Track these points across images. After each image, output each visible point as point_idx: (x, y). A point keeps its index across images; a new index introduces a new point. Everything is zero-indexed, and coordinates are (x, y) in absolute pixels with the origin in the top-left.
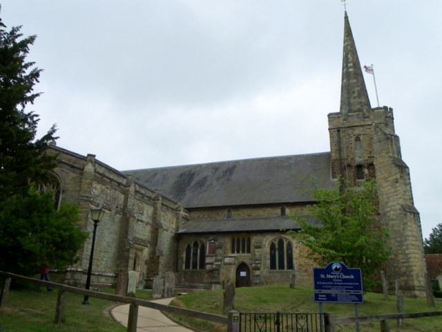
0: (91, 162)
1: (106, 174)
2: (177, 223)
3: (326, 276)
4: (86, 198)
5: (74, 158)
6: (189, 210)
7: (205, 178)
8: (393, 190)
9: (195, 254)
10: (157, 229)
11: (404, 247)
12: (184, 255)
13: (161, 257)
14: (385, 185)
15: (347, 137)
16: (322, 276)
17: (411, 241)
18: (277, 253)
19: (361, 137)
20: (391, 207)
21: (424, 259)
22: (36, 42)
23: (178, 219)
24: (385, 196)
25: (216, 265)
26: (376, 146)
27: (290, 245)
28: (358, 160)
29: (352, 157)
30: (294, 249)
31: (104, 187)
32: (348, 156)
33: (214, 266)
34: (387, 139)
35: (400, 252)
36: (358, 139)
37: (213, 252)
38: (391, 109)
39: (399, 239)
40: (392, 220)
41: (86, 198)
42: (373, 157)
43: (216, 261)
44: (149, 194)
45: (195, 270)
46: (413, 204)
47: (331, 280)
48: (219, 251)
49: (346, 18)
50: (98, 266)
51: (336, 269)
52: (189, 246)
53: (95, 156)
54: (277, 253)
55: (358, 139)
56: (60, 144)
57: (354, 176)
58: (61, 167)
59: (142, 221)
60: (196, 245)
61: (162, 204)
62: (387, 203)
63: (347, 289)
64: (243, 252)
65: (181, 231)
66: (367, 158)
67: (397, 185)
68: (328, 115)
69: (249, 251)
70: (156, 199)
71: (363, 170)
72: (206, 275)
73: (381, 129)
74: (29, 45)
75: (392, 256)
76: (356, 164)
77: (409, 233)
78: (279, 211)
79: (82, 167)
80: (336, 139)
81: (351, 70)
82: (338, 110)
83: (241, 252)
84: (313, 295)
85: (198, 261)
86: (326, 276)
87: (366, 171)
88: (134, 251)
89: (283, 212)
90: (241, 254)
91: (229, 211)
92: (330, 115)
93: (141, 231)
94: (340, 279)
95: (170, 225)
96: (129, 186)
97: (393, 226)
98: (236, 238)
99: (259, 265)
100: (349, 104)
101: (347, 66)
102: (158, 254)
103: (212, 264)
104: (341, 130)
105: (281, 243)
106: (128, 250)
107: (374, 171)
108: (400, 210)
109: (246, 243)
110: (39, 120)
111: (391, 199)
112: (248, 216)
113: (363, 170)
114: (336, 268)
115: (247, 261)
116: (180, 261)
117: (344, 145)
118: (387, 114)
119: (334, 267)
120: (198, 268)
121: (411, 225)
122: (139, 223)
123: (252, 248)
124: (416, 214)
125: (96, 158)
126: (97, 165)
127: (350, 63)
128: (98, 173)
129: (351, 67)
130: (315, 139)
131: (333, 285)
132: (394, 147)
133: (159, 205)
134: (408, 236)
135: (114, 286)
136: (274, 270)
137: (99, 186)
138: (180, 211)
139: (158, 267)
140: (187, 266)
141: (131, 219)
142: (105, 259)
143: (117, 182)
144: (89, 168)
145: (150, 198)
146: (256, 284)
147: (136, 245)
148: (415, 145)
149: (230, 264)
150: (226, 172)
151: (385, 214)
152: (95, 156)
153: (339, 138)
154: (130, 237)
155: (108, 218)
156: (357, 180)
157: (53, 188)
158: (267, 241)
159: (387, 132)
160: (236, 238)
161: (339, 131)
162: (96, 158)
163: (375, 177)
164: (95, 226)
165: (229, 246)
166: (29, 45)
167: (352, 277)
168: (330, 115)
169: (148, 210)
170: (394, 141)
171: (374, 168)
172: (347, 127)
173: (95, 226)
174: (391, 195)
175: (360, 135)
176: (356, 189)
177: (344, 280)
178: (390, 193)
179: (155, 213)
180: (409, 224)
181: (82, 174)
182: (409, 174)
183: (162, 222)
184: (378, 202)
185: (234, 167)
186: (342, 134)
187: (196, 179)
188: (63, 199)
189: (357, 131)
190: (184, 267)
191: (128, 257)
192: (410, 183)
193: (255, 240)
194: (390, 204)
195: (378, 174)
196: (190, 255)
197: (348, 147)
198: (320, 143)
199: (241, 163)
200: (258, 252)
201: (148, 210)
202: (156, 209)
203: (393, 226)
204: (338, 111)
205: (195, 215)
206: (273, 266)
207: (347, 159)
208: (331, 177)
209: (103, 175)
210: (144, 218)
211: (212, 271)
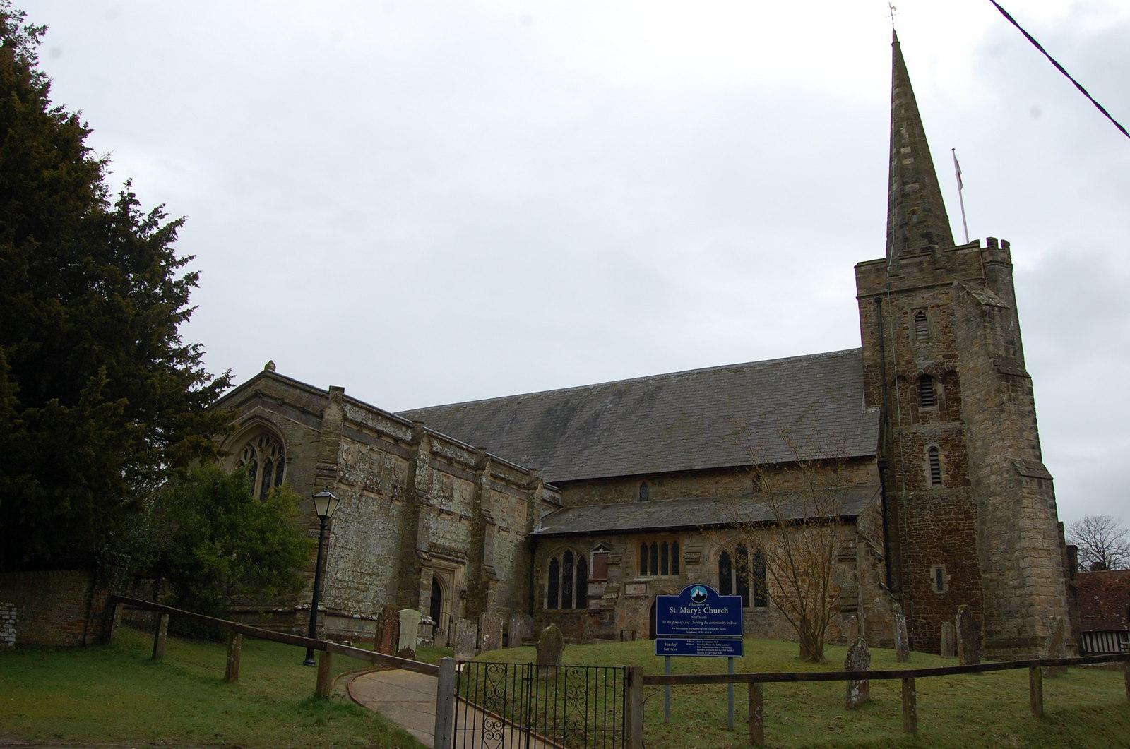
0: (336, 400)
1: (367, 422)
2: (530, 514)
3: (678, 609)
4: (326, 473)
5: (307, 395)
6: (561, 486)
7: (597, 416)
8: (994, 429)
9: (568, 578)
10: (483, 529)
11: (1017, 554)
13: (491, 584)
14: (977, 417)
16: (673, 610)
19: (929, 314)
22: (186, 224)
23: (531, 506)
26: (960, 332)
27: (759, 556)
28: (922, 364)
29: (907, 357)
31: (365, 449)
32: (899, 356)
33: (603, 602)
34: (983, 314)
36: (921, 317)
37: (603, 573)
38: (1006, 244)
39: (1006, 536)
40: (994, 494)
41: (326, 473)
42: (956, 356)
44: (465, 457)
45: (568, 611)
46: (1040, 458)
47: (687, 617)
49: (896, 45)
50: (359, 603)
51: (698, 598)
52: (555, 562)
53: (343, 389)
56: (278, 371)
57: (914, 400)
58: (285, 413)
59: (450, 513)
60: (569, 558)
61: (495, 477)
63: (714, 632)
64: (665, 572)
65: (538, 530)
66: (940, 359)
67: (1003, 416)
69: (676, 571)
70: (479, 467)
71: (934, 387)
72: (590, 621)
73: (968, 294)
74: (178, 229)
75: (994, 575)
77: (1028, 523)
79: (319, 413)
80: (873, 319)
81: (905, 162)
83: (659, 572)
85: (574, 593)
86: (678, 609)
87: (940, 388)
88: (431, 572)
90: (660, 576)
91: (644, 486)
92: (859, 267)
93: (448, 531)
94: (703, 614)
95: (511, 518)
96: (418, 444)
101: (898, 153)
102: (485, 579)
103: (599, 597)
104: (884, 298)
105: (742, 551)
106: (418, 571)
107: (957, 390)
113: (934, 387)
114: (698, 595)
116: (536, 594)
118: (993, 261)
120: (574, 606)
121: (1032, 508)
122: (444, 516)
123: (682, 561)
124: (1045, 481)
128: (352, 421)
129: (907, 156)
130: (823, 319)
132: (999, 331)
133: (486, 480)
134: (1023, 530)
135: (378, 641)
137: (353, 448)
138: (535, 489)
140: (552, 604)
141: (424, 509)
142: (374, 588)
143: (392, 437)
144: (333, 413)
145: (465, 465)
147: (435, 561)
149: (637, 598)
150: (641, 401)
151: (979, 483)
152: (343, 389)
153: (880, 316)
155: (375, 509)
156: (921, 409)
157: (273, 455)
158: (711, 550)
160: (659, 543)
161: (878, 301)
163: (958, 400)
165: (634, 560)
166: (178, 229)
167: (726, 611)
169: (462, 490)
170: (998, 318)
171: (957, 382)
172: (898, 292)
175: (926, 308)
176: (919, 428)
177: (711, 617)
179: (477, 495)
180: (1026, 502)
181: (320, 425)
182: (1031, 392)
185: (658, 389)
186: (884, 307)
187: (580, 418)
188: (289, 474)
189: (919, 300)
190: (546, 606)
191: (419, 583)
192: (1033, 412)
193: (687, 546)
194: (988, 461)
195: (965, 395)
196: (556, 582)
197: (899, 337)
198: (834, 325)
199: (674, 380)
200: (691, 572)
201: (462, 490)
202: (479, 487)
203: (995, 508)
204: (884, 256)
205: (573, 495)
207: (898, 364)
209: (361, 426)
210: (455, 506)
211: (598, 613)
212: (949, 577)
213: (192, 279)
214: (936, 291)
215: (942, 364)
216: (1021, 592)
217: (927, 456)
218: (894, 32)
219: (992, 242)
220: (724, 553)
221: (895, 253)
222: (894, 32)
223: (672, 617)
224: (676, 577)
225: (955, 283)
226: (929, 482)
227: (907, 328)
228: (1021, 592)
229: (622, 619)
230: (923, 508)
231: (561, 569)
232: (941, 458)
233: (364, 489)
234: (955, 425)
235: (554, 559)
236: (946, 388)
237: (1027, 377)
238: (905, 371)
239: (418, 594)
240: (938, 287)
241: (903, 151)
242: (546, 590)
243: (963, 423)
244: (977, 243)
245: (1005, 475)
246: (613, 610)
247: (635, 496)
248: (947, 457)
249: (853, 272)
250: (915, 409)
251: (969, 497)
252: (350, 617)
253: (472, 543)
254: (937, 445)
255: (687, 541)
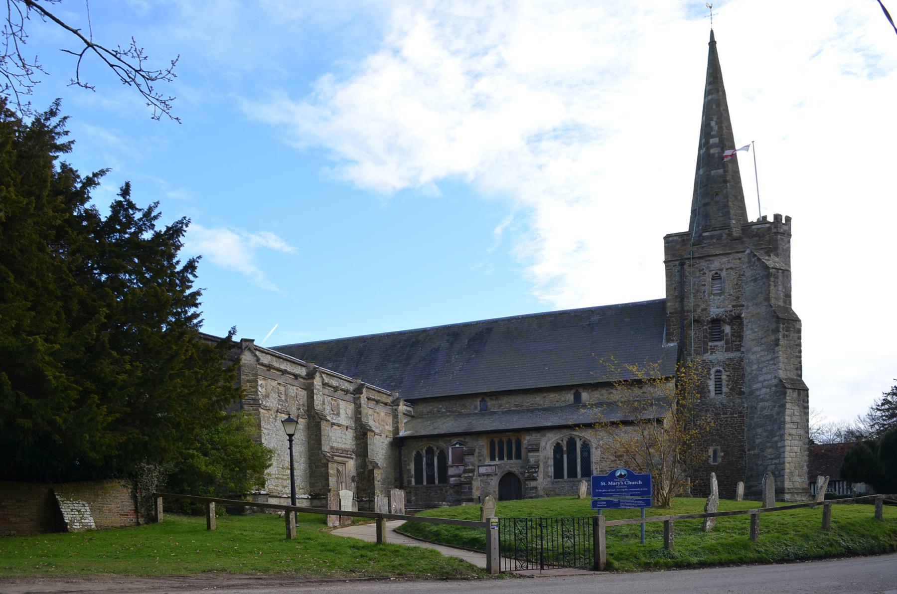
0: (249, 349)
3: (607, 483)
8: (769, 357)
9: (430, 465)
11: (776, 438)
12: (412, 467)
13: (376, 471)
15: (698, 274)
16: (603, 484)
17: (789, 428)
18: (565, 456)
19: (723, 274)
20: (762, 382)
21: (807, 453)
23: (395, 417)
24: (755, 367)
25: (466, 478)
27: (586, 447)
28: (714, 311)
29: (703, 306)
30: (593, 450)
31: (274, 383)
33: (462, 479)
35: (769, 444)
36: (717, 277)
37: (459, 459)
38: (788, 219)
40: (762, 400)
42: (743, 306)
43: (465, 471)
46: (800, 376)
48: (469, 459)
49: (712, 44)
51: (621, 476)
54: (565, 456)
55: (717, 277)
57: (705, 337)
59: (339, 425)
60: (430, 452)
61: (368, 399)
62: (756, 376)
64: (510, 458)
65: (402, 433)
66: (730, 308)
68: (665, 238)
69: (519, 456)
73: (759, 259)
76: (709, 318)
78: (570, 397)
81: (712, 151)
82: (684, 227)
83: (505, 459)
84: (590, 503)
85: (436, 475)
87: (727, 329)
89: (578, 397)
91: (483, 400)
92: (668, 239)
93: (339, 438)
95: (382, 425)
96: (313, 378)
97: (763, 409)
98: (496, 441)
99: (535, 475)
100: (706, 216)
101: (707, 142)
104: (687, 262)
105: (572, 443)
106: (326, 466)
108: (776, 386)
109: (514, 446)
110: (200, 322)
111: (765, 370)
112: (517, 406)
113: (725, 329)
115: (515, 470)
117: (690, 289)
118: (774, 235)
119: (618, 474)
120: (437, 482)
121: (791, 410)
122: (335, 427)
123: (523, 451)
124: (803, 391)
125: (255, 343)
126: (257, 353)
127: (713, 137)
131: (616, 492)
136: (560, 480)
138: (398, 405)
139: (373, 484)
140: (419, 480)
145: (346, 392)
146: (531, 498)
147: (335, 458)
148: (813, 288)
149: (488, 475)
151: (752, 393)
152: (253, 340)
154: (326, 448)
156: (710, 344)
158: (548, 444)
159: (770, 263)
160: (496, 441)
161: (682, 264)
162: (255, 343)
164: (291, 441)
165: (486, 451)
167: (640, 482)
168: (668, 239)
169: (346, 409)
170: (780, 278)
171: (741, 324)
172: (699, 258)
173: (291, 441)
174: (765, 364)
175: (721, 270)
176: (707, 357)
177: (629, 486)
178: (764, 362)
183: (371, 423)
184: (744, 374)
185: (489, 330)
186: (687, 269)
190: (413, 483)
194: (761, 378)
198: (649, 283)
204: (687, 230)
205: (423, 408)
206: (558, 473)
207: (695, 311)
208: (664, 341)
211: (459, 485)
212: (722, 454)
213: (191, 266)
214: (731, 257)
215: (731, 311)
216: (777, 461)
217: (712, 376)
218: (712, 32)
219: (777, 217)
220: (558, 444)
221: (698, 226)
222: (712, 32)
223: (604, 487)
224: (519, 461)
225: (748, 251)
226: (713, 394)
227: (704, 285)
228: (777, 461)
229: (477, 490)
230: (706, 411)
231: (424, 459)
232: (724, 377)
233: (277, 411)
234: (737, 354)
235: (418, 452)
236: (732, 329)
237: (797, 320)
238: (700, 317)
239: (328, 480)
240: (730, 253)
241: (712, 141)
242: (413, 472)
243: (743, 352)
244: (765, 218)
245: (773, 388)
246: (471, 484)
247: (476, 408)
248: (728, 376)
249: (663, 241)
250: (706, 343)
251: (743, 402)
252: (280, 497)
253: (357, 445)
254: (721, 369)
255: (528, 438)
